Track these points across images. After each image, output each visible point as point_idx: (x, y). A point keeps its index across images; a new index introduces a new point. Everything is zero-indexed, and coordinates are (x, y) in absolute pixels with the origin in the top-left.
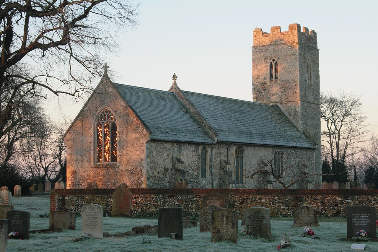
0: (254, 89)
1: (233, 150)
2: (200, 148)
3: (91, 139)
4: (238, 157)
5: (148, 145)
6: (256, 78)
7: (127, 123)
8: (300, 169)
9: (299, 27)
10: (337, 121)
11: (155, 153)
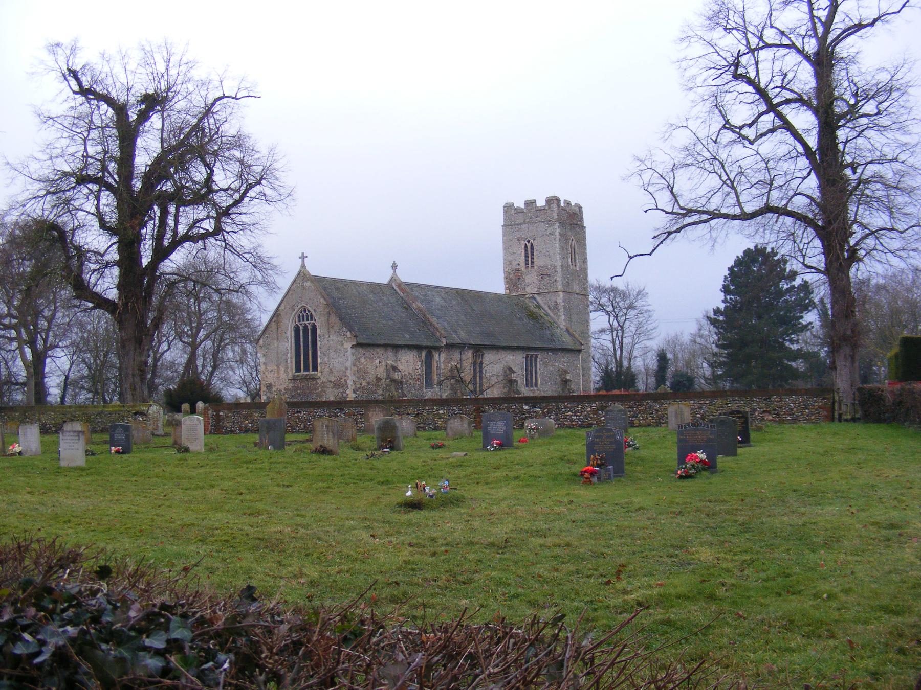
0: (506, 278)
1: (469, 354)
2: (424, 354)
3: (288, 345)
4: (475, 364)
5: (353, 350)
6: (508, 263)
7: (329, 326)
8: (560, 375)
9: (558, 200)
10: (621, 314)
11: (363, 360)
